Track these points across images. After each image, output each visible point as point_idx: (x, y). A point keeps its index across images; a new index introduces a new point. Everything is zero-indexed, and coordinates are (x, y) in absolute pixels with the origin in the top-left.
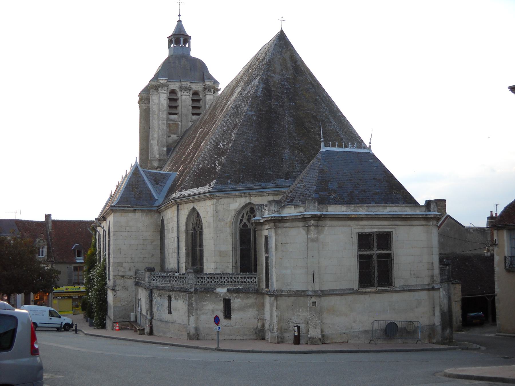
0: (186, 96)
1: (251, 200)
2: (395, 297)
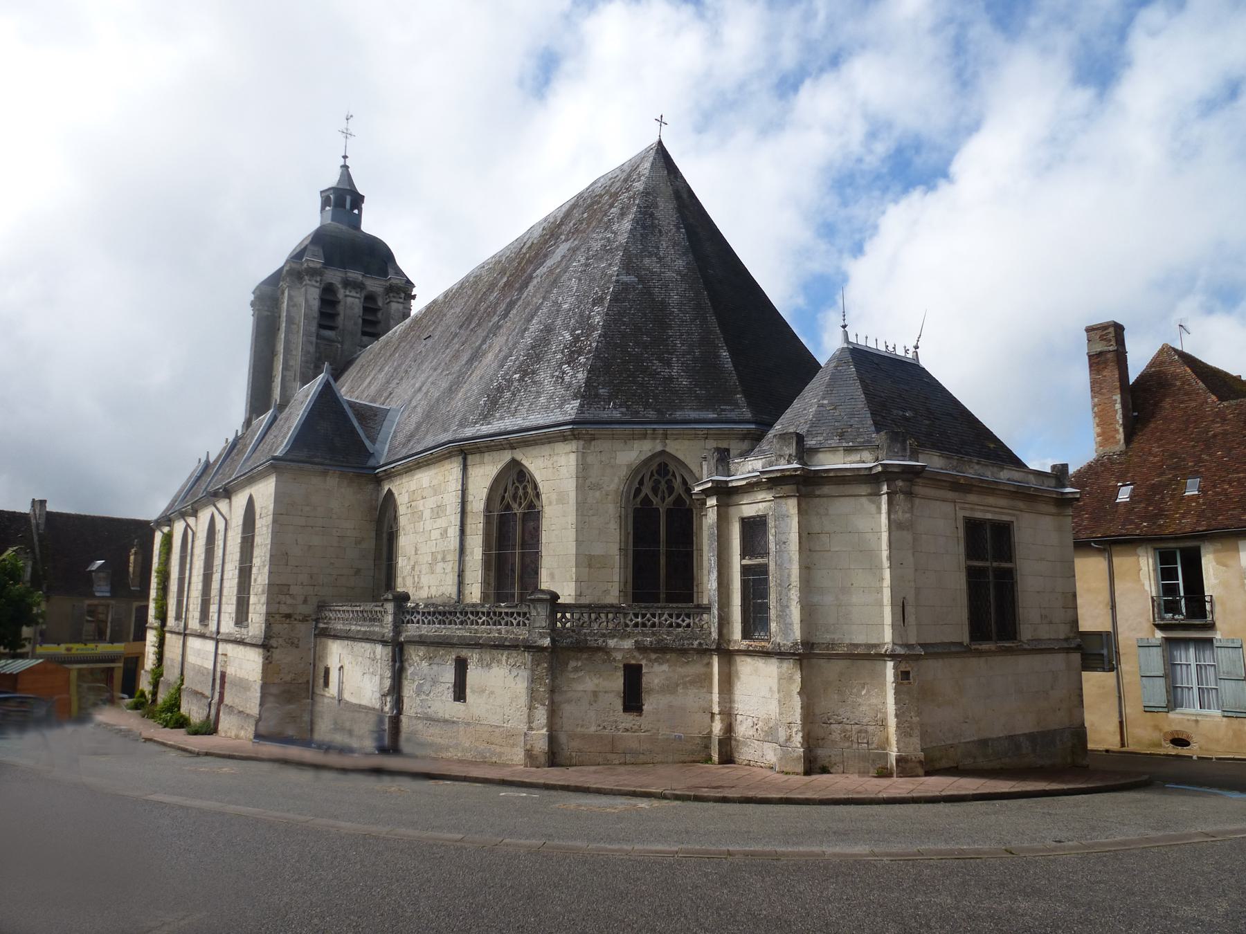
1: (666, 445)
2: (1024, 664)
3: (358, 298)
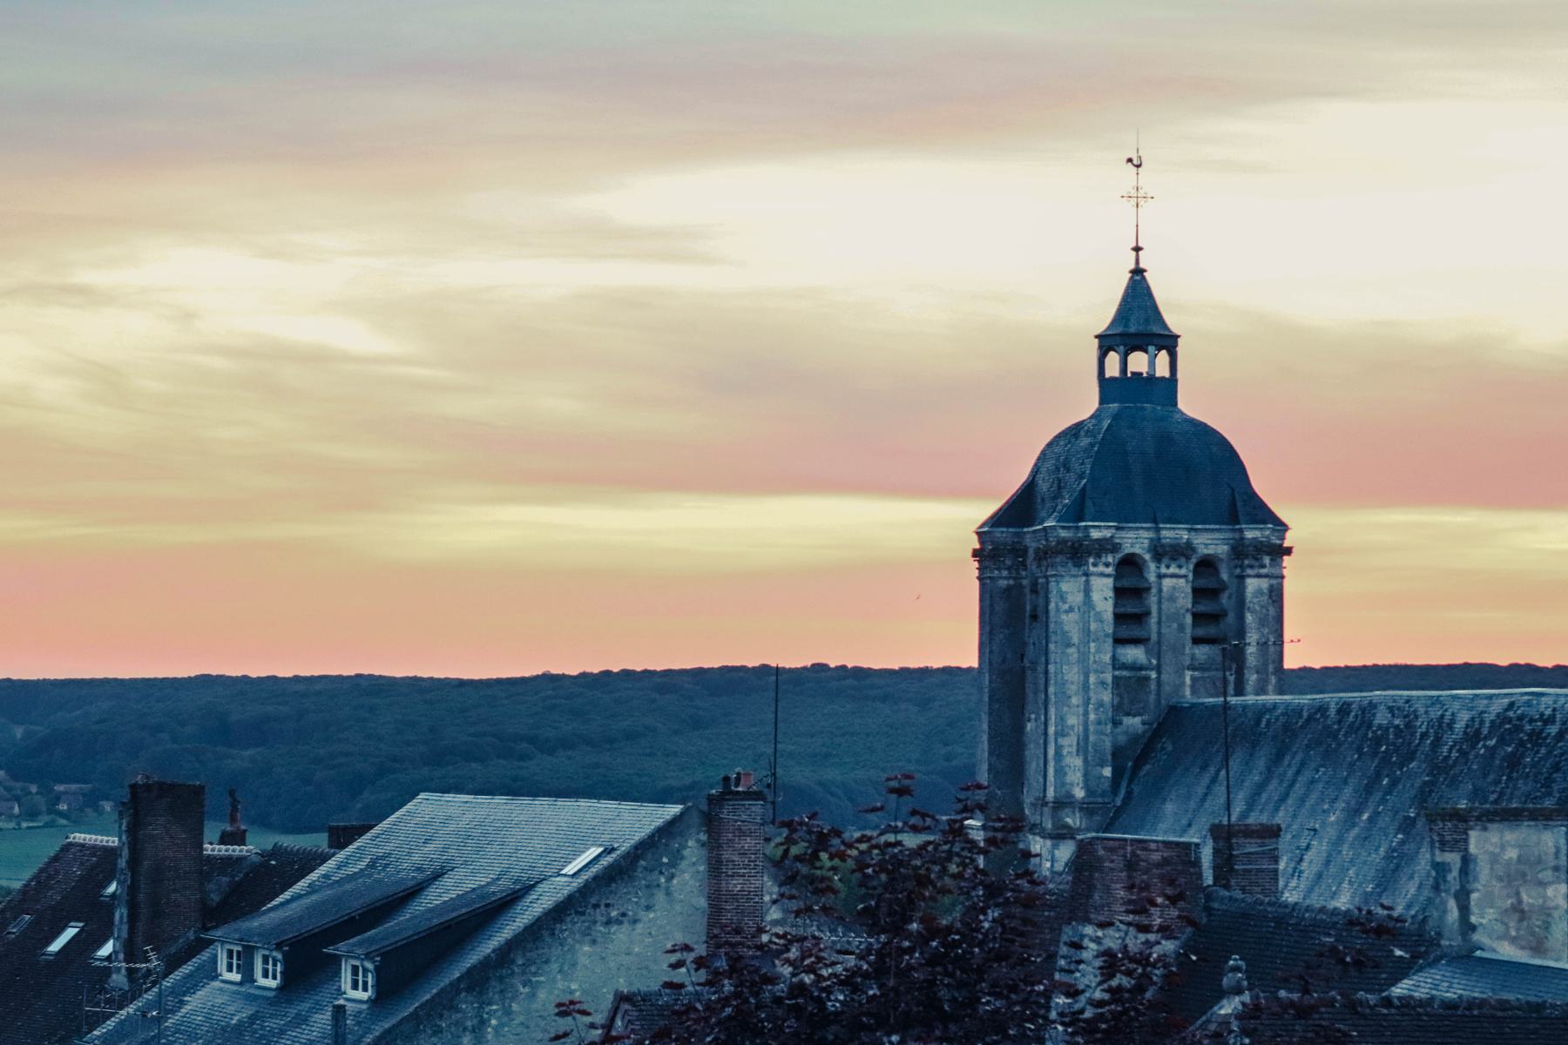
0: (1174, 580)
3: (1185, 576)
